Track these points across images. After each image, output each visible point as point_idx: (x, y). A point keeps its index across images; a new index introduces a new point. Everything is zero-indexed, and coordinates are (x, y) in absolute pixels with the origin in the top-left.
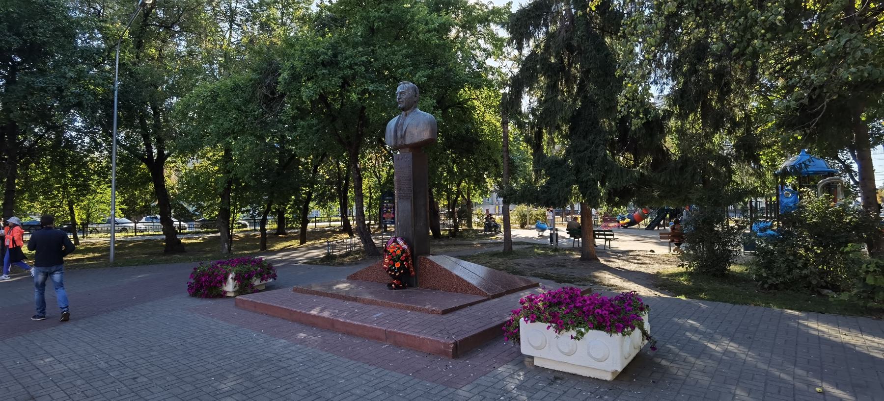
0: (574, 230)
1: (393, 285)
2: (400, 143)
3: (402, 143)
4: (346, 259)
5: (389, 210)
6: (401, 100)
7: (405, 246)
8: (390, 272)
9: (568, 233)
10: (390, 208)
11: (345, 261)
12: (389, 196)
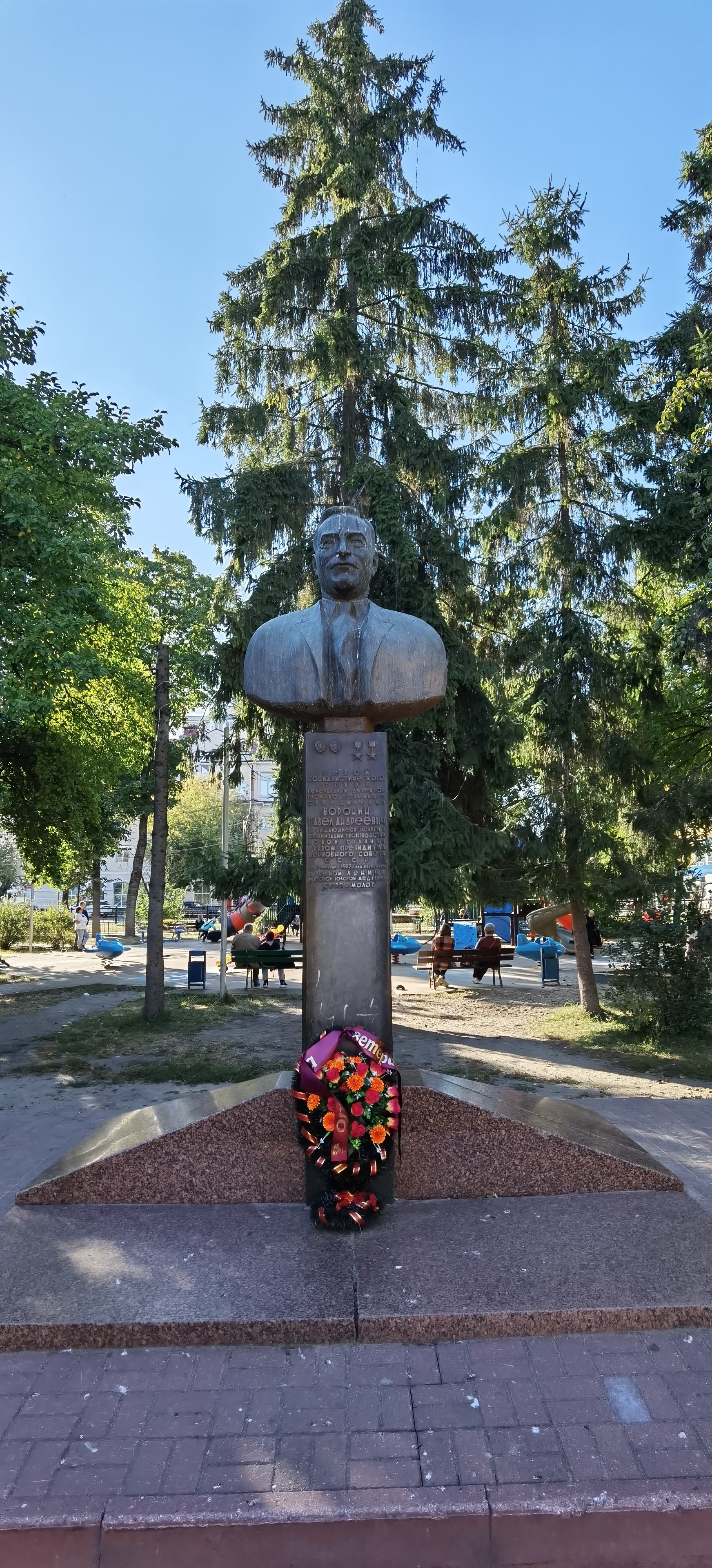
0: (251, 952)
1: (356, 1217)
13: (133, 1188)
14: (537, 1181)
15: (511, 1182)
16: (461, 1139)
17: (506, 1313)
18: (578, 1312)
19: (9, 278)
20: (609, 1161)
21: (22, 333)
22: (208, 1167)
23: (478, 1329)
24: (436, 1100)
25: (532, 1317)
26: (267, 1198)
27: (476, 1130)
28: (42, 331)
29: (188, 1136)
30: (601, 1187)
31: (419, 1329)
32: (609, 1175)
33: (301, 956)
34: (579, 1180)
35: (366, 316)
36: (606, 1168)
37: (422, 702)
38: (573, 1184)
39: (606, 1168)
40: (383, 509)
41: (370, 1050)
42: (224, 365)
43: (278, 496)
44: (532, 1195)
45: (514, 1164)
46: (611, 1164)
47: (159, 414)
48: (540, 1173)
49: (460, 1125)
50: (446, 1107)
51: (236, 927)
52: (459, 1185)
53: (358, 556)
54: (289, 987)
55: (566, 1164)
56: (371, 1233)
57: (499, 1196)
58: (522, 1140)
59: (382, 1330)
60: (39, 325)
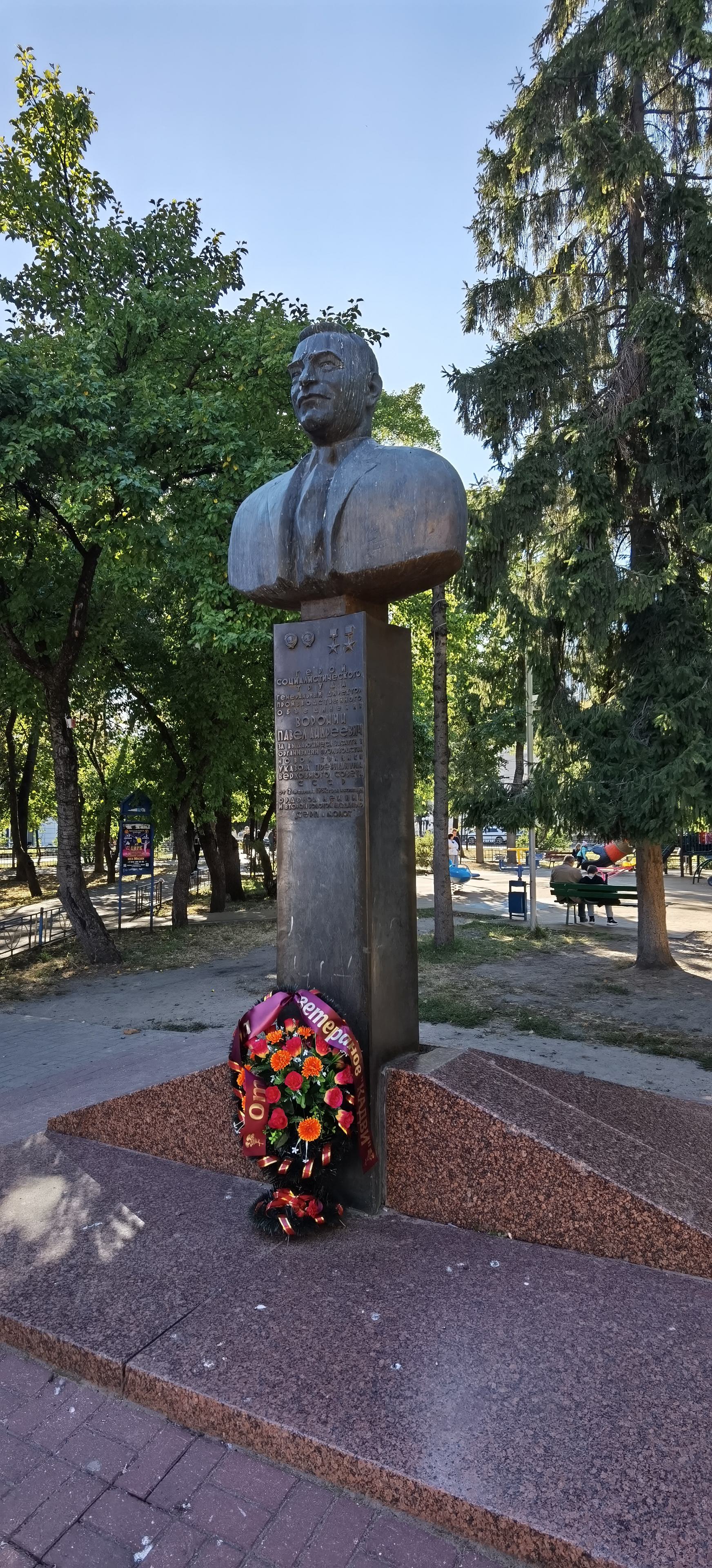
0: (570, 885)
1: (286, 1224)
2: (311, 571)
3: (320, 568)
4: (31, 975)
5: (139, 840)
6: (315, 390)
7: (339, 1036)
8: (267, 1162)
9: (552, 893)
10: (141, 835)
11: (27, 983)
12: (140, 806)
13: (135, 1134)
14: (569, 1230)
15: (531, 1222)
16: (469, 1151)
17: (289, 1428)
18: (382, 1468)
19: (198, 205)
20: (678, 1227)
21: (226, 259)
22: (198, 1127)
23: (251, 1436)
24: (438, 1094)
25: (318, 1449)
26: (252, 1175)
27: (488, 1144)
28: (243, 250)
29: (180, 1089)
30: (664, 1262)
31: (187, 1407)
32: (679, 1248)
33: (635, 893)
34: (631, 1243)
35: (659, 112)
36: (672, 1236)
37: (414, 564)
38: (622, 1248)
39: (672, 1236)
40: (658, 352)
41: (314, 1021)
42: (483, 236)
43: (535, 367)
44: (560, 1247)
45: (537, 1199)
46: (680, 1231)
47: (355, 303)
48: (574, 1220)
49: (467, 1132)
50: (450, 1107)
51: (612, 858)
52: (464, 1210)
53: (328, 383)
54: (619, 925)
55: (612, 1217)
56: (298, 1249)
57: (515, 1238)
58: (549, 1169)
59: (148, 1391)
60: (242, 246)
